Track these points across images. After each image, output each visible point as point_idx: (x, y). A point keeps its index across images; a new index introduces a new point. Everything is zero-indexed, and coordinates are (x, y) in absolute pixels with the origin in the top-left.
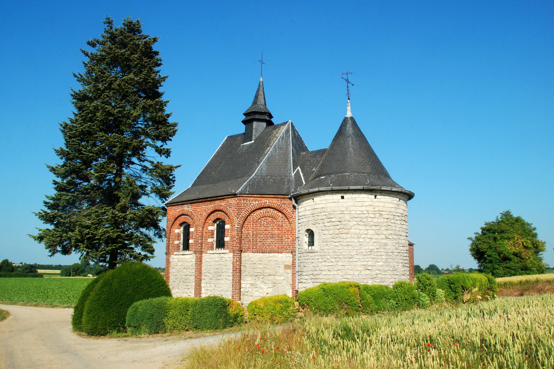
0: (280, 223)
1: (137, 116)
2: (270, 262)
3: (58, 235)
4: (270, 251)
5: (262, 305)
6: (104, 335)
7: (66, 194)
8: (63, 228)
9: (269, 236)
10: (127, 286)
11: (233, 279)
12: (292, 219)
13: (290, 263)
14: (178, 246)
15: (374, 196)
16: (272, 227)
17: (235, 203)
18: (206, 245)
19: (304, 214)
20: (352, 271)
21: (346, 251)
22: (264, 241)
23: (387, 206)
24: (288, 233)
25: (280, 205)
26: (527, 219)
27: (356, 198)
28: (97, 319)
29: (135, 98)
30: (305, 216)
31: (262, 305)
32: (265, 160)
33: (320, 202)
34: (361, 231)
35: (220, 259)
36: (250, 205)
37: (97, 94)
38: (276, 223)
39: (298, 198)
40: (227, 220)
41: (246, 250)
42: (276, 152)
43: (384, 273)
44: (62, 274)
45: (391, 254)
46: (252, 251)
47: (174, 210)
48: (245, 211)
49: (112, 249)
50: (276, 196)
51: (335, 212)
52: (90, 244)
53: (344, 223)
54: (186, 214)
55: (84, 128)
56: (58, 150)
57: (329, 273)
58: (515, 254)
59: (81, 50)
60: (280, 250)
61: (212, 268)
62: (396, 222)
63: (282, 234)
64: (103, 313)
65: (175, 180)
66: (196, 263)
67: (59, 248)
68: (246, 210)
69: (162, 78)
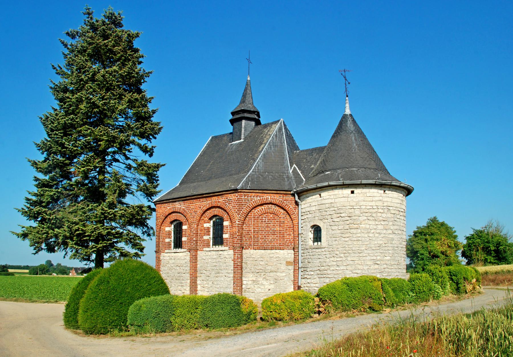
0: (282, 220)
1: (123, 110)
2: (272, 258)
3: (44, 232)
4: (272, 247)
5: (279, 302)
6: (104, 334)
7: (50, 190)
8: (48, 224)
10: (126, 284)
11: (234, 277)
13: (292, 260)
14: (169, 244)
15: (383, 191)
16: (273, 223)
17: (236, 199)
18: (202, 242)
19: (309, 210)
20: (362, 266)
21: (356, 246)
23: (394, 201)
26: (450, 225)
27: (366, 193)
28: (95, 318)
29: (120, 92)
30: (311, 212)
31: (278, 301)
32: (261, 157)
33: (328, 197)
34: (371, 226)
35: (218, 256)
36: (251, 201)
37: (80, 85)
39: (302, 194)
40: (225, 216)
41: (247, 247)
42: (271, 149)
43: (390, 267)
44: (30, 273)
45: (396, 248)
46: (254, 247)
47: (164, 207)
48: (246, 207)
49: (103, 246)
50: (279, 192)
51: (344, 207)
52: (80, 240)
54: (178, 211)
55: (68, 120)
56: (38, 144)
57: (337, 269)
58: (442, 253)
59: (60, 40)
61: (209, 265)
62: (401, 217)
64: (102, 311)
65: (158, 180)
66: (190, 261)
67: (43, 246)
68: (248, 206)
69: (146, 73)
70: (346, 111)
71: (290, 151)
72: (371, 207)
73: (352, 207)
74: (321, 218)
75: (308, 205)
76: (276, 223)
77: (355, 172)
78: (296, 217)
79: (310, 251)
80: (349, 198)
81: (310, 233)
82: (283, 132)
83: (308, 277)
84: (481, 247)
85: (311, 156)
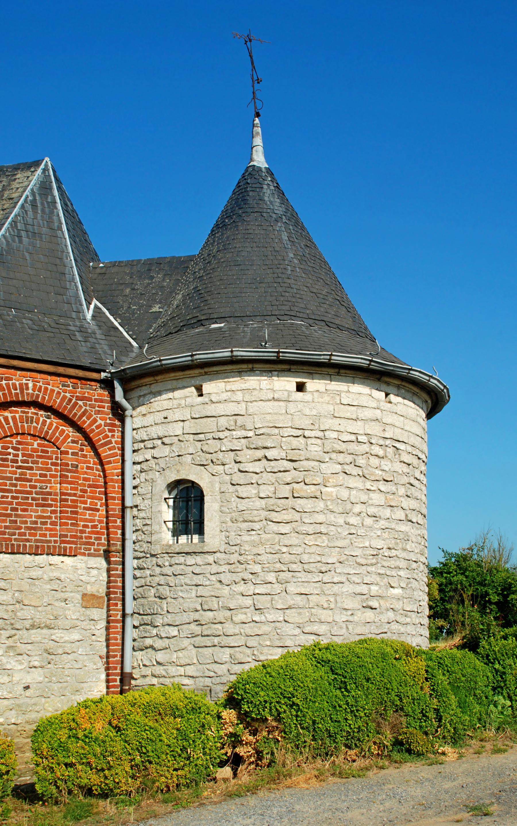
2: (37, 582)
4: (37, 547)
9: (33, 499)
12: (110, 449)
15: (383, 394)
19: (161, 434)
20: (330, 612)
22: (17, 516)
24: (95, 492)
25: (70, 400)
27: (339, 393)
30: (166, 440)
31: (99, 725)
34: (354, 492)
38: (57, 458)
42: (20, 242)
50: (61, 370)
51: (276, 431)
53: (306, 464)
57: (257, 618)
60: (68, 546)
63: (75, 495)
70: (255, 157)
71: (79, 259)
72: (353, 438)
73: (300, 432)
74: (204, 458)
75: (159, 417)
76: (50, 470)
77: (304, 329)
78: (115, 455)
79: (166, 560)
80: (291, 405)
81: (164, 506)
82: (54, 197)
83: (159, 644)
84: (470, 593)
85: (147, 281)
